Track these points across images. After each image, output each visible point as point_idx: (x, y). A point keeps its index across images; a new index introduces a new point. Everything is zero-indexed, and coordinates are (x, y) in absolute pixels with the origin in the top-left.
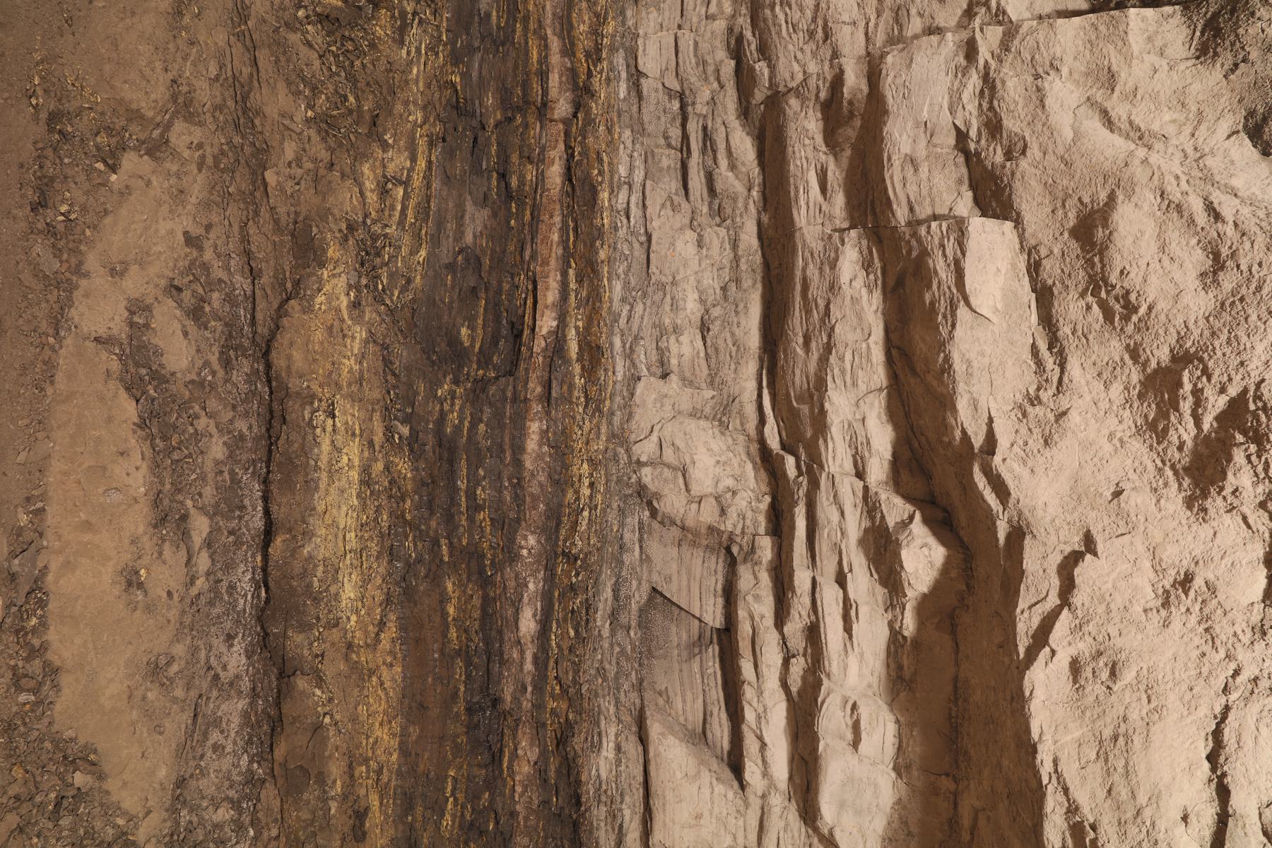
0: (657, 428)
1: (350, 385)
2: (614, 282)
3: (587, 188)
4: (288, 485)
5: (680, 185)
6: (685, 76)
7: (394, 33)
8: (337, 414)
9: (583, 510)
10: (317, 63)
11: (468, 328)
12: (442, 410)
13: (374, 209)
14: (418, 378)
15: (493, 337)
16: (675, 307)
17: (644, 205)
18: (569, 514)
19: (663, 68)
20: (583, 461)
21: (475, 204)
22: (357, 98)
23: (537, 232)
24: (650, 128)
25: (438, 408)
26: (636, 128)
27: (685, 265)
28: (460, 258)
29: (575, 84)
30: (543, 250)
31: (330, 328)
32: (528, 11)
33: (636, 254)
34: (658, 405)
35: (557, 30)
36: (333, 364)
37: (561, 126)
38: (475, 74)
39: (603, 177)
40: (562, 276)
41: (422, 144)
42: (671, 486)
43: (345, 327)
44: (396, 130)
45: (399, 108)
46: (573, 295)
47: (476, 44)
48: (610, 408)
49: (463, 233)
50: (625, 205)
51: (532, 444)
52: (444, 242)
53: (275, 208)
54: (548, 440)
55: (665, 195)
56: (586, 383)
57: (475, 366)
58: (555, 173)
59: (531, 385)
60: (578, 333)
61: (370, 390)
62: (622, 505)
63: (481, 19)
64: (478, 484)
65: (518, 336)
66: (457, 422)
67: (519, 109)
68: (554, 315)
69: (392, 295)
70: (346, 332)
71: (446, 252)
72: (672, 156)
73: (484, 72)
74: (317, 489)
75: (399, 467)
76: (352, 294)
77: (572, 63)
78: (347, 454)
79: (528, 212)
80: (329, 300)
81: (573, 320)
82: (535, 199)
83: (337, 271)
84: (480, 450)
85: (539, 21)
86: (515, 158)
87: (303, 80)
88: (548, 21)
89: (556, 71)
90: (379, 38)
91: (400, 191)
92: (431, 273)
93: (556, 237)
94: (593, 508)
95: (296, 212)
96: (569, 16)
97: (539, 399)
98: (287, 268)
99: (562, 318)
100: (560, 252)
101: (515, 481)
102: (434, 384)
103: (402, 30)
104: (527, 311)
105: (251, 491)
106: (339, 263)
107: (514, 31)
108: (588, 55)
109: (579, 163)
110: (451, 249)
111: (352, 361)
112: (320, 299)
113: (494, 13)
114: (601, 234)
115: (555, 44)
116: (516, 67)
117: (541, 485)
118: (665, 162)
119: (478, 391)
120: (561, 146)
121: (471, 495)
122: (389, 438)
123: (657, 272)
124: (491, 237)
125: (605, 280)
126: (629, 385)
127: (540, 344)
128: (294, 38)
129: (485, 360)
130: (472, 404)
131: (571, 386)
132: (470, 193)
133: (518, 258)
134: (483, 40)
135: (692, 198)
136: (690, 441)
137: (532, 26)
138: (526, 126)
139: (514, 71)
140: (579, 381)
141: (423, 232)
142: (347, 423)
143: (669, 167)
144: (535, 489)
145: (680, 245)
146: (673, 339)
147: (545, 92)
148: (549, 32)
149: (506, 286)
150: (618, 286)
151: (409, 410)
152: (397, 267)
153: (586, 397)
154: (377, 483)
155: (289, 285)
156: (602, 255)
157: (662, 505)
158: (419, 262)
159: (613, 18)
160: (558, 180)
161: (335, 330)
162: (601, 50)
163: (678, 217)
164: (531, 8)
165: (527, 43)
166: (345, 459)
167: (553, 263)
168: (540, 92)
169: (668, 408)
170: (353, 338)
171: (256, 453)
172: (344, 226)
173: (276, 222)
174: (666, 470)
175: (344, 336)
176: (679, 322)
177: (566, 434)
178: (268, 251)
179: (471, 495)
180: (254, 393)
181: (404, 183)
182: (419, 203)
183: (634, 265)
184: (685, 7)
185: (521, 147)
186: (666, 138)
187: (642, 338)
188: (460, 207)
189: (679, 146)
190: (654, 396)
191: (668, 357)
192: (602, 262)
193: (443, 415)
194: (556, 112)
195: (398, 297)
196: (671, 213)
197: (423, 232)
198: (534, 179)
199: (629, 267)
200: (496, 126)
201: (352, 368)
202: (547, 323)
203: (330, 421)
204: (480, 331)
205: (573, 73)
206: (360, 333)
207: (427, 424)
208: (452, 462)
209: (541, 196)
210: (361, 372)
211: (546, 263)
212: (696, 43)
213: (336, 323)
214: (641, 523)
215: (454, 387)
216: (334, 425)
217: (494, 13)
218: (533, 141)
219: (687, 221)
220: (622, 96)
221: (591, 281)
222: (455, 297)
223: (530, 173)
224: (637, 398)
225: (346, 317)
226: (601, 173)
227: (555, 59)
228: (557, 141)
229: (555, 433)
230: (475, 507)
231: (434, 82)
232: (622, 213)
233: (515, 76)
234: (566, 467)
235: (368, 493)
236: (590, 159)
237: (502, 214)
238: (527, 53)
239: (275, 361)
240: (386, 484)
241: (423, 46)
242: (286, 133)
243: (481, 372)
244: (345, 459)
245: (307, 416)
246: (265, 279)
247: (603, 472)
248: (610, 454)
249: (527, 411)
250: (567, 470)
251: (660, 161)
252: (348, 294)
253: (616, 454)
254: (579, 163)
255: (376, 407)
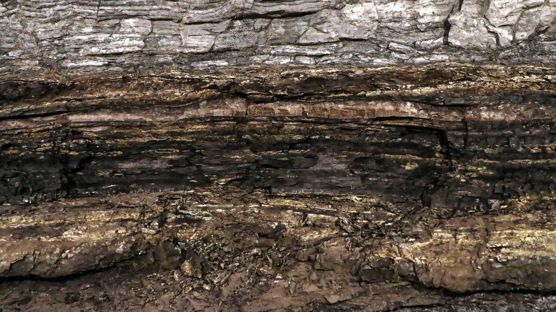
0: (492, 29)
1: (475, 238)
2: (375, 64)
3: (308, 85)
4: (545, 277)
5: (300, 19)
6: (221, 16)
7: (193, 227)
8: (500, 245)
9: (547, 79)
10: (238, 275)
11: (406, 165)
12: (476, 178)
13: (332, 232)
14: (454, 195)
15: (410, 148)
16: (398, 19)
17: (316, 44)
18: (548, 89)
19: (209, 33)
20: (511, 81)
21: (314, 164)
22: (251, 248)
23: (337, 119)
24: (252, 42)
25: (475, 181)
26: (249, 53)
27: (368, 12)
28: (356, 172)
29: (220, 97)
30: (351, 115)
31: (437, 253)
32: (167, 133)
33: (351, 49)
34: (472, 29)
35: (179, 112)
36: (462, 250)
37: (251, 106)
38: (219, 169)
39: (301, 73)
40: (371, 101)
41: (273, 203)
42: (534, 17)
43: (435, 243)
44: (267, 221)
45: (250, 220)
46: (386, 92)
47: (195, 168)
48: (470, 63)
49: (339, 171)
50: (312, 59)
51: (499, 116)
52: (345, 184)
53: (352, 295)
54: (494, 105)
55: (311, 29)
56: (451, 81)
57: (433, 159)
58: (292, 108)
59: (451, 119)
60: (416, 87)
61: (478, 224)
62: (538, 53)
63: (174, 167)
64: (529, 152)
65: (410, 129)
66: (485, 168)
67: (239, 137)
68: (402, 105)
69: (391, 216)
70: (438, 243)
71: (353, 182)
72: (276, 25)
73: (217, 162)
74: (547, 258)
75: (523, 204)
76: (411, 240)
77: (203, 100)
78: (525, 238)
79: (320, 127)
80: (417, 255)
81: (407, 91)
82: (311, 122)
83: (397, 250)
84: (504, 152)
85: (174, 124)
86: (279, 138)
87: (256, 283)
88: (172, 118)
89: (211, 111)
90: (199, 236)
91: (310, 215)
92: (369, 192)
93: (341, 106)
94: (545, 72)
95: (351, 282)
96: (167, 103)
97: (462, 112)
98: (391, 285)
99: (404, 99)
100: (352, 103)
101: (524, 127)
102: (457, 184)
103: (191, 221)
104: (397, 124)
105: (544, 304)
106: (392, 249)
107: (183, 142)
108: (198, 89)
109: (290, 91)
110: (351, 179)
111: (460, 237)
112: (417, 261)
113: (170, 157)
114: (345, 75)
115: (190, 113)
116: (210, 140)
117: (527, 109)
118: (281, 30)
119: (458, 155)
120: (270, 105)
121: (536, 156)
122: (506, 212)
123: (369, 33)
124: (339, 151)
125: (377, 69)
126: (452, 51)
127: (423, 115)
128: (226, 291)
129: (429, 152)
130: (472, 157)
131: (456, 91)
132: (308, 168)
133: (354, 132)
134: (191, 164)
135: (316, 9)
136: (509, 4)
137: (177, 129)
138: (252, 131)
139: (213, 141)
140: (451, 85)
141: (338, 198)
142: (505, 238)
143: (284, 27)
144: (530, 113)
145: (353, 17)
146: (421, 20)
147: (227, 118)
148: (181, 117)
149: (375, 140)
150: (378, 61)
151: (478, 200)
152: (372, 214)
153: (463, 80)
154: (542, 218)
155: (403, 283)
156: (359, 72)
157: (546, 23)
158: (361, 201)
159: (169, 71)
160: (297, 106)
161: (438, 250)
162: (194, 79)
163: (331, 19)
164: (164, 131)
165: (192, 133)
166: (528, 239)
167: (361, 107)
168: (227, 122)
169: (475, 22)
170: (441, 237)
171: (519, 301)
172: (357, 249)
173: (361, 294)
174: (520, 22)
175: (441, 243)
176: (409, 16)
177: (489, 93)
178: (381, 298)
179: (536, 156)
180: (478, 304)
181: (304, 213)
182: (317, 202)
183: (359, 50)
184: (166, 17)
185: (271, 134)
186: (261, 29)
187: (414, 43)
188: (318, 174)
189: (269, 20)
190: (464, 32)
191: (433, 23)
192: (365, 72)
193: (480, 177)
194: (240, 110)
195: (392, 212)
196: (326, 25)
197: (338, 198)
198: (295, 123)
199: (361, 53)
200: (255, 152)
201: (464, 237)
202: (409, 109)
203: (503, 250)
204: (407, 157)
205: (211, 99)
206: (438, 233)
207: (487, 188)
208: (513, 170)
209: (309, 118)
210: (466, 231)
211: (361, 112)
212: (196, 8)
213: (433, 249)
214: (546, 40)
215: (457, 171)
216: (506, 247)
217: (170, 157)
218: (265, 126)
219: (334, 12)
220: (226, 64)
221: (377, 79)
222: (385, 174)
223: (293, 126)
224: (464, 45)
225: (428, 243)
226: (297, 75)
227: (202, 112)
228: (265, 109)
229: (490, 101)
230: (544, 154)
231: (225, 197)
232: (317, 61)
233: (216, 140)
234: (513, 92)
235: (549, 223)
236: (287, 83)
237: (321, 145)
238: (199, 132)
239: (465, 288)
240: (540, 212)
241: (201, 206)
242: (298, 291)
243: (437, 155)
244: (528, 239)
245: (498, 266)
246: (402, 299)
247: (519, 67)
248: (504, 62)
249: (474, 121)
250: (516, 92)
251: (279, 34)
252: (412, 242)
253: (505, 58)
254: (290, 91)
255: (490, 219)
